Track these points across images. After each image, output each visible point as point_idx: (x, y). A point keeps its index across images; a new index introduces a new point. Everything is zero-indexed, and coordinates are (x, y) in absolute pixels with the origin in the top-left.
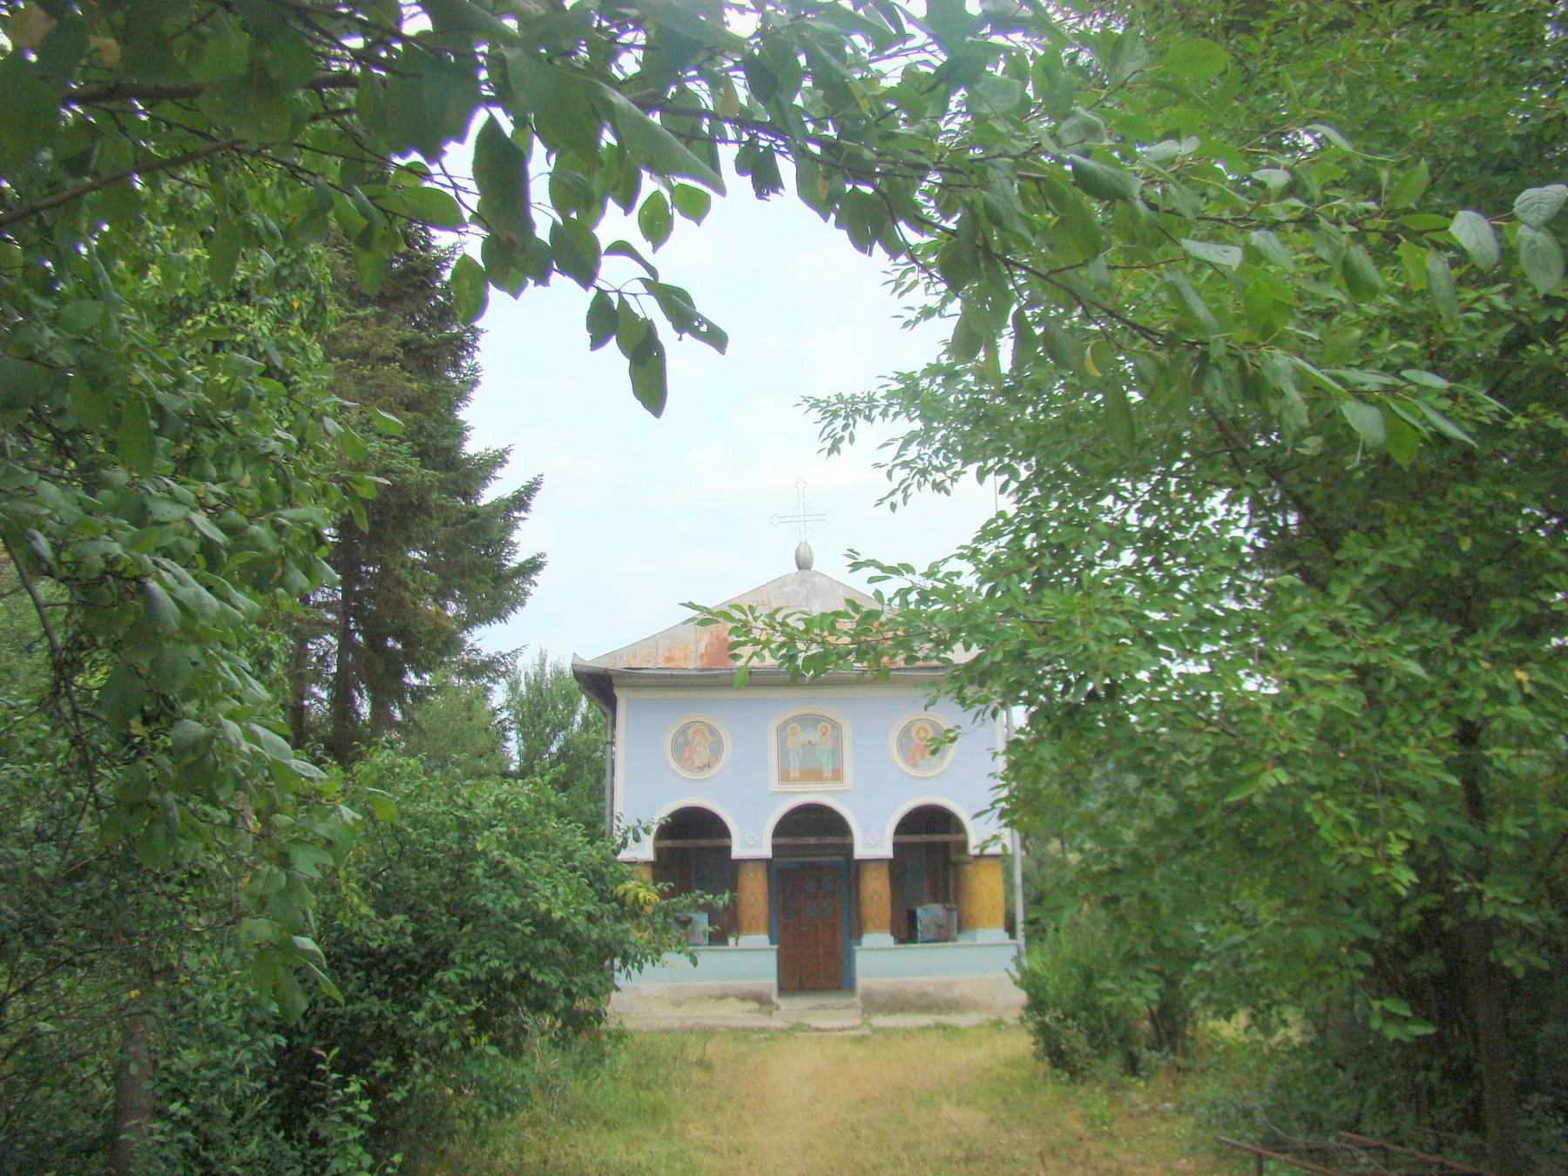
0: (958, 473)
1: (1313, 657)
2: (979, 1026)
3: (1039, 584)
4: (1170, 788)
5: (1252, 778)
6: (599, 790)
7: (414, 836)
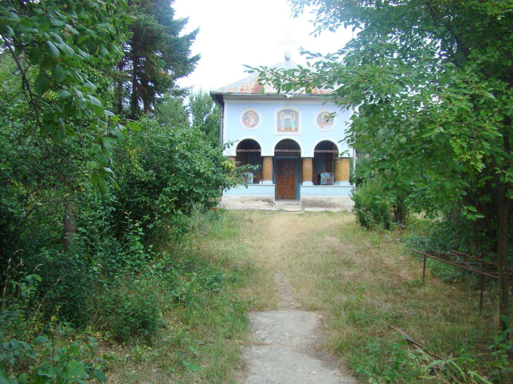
0: (338, 25)
1: (457, 91)
2: (339, 212)
3: (365, 62)
4: (405, 133)
5: (433, 129)
6: (218, 133)
7: (156, 145)
